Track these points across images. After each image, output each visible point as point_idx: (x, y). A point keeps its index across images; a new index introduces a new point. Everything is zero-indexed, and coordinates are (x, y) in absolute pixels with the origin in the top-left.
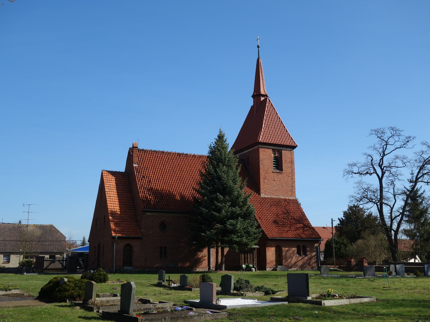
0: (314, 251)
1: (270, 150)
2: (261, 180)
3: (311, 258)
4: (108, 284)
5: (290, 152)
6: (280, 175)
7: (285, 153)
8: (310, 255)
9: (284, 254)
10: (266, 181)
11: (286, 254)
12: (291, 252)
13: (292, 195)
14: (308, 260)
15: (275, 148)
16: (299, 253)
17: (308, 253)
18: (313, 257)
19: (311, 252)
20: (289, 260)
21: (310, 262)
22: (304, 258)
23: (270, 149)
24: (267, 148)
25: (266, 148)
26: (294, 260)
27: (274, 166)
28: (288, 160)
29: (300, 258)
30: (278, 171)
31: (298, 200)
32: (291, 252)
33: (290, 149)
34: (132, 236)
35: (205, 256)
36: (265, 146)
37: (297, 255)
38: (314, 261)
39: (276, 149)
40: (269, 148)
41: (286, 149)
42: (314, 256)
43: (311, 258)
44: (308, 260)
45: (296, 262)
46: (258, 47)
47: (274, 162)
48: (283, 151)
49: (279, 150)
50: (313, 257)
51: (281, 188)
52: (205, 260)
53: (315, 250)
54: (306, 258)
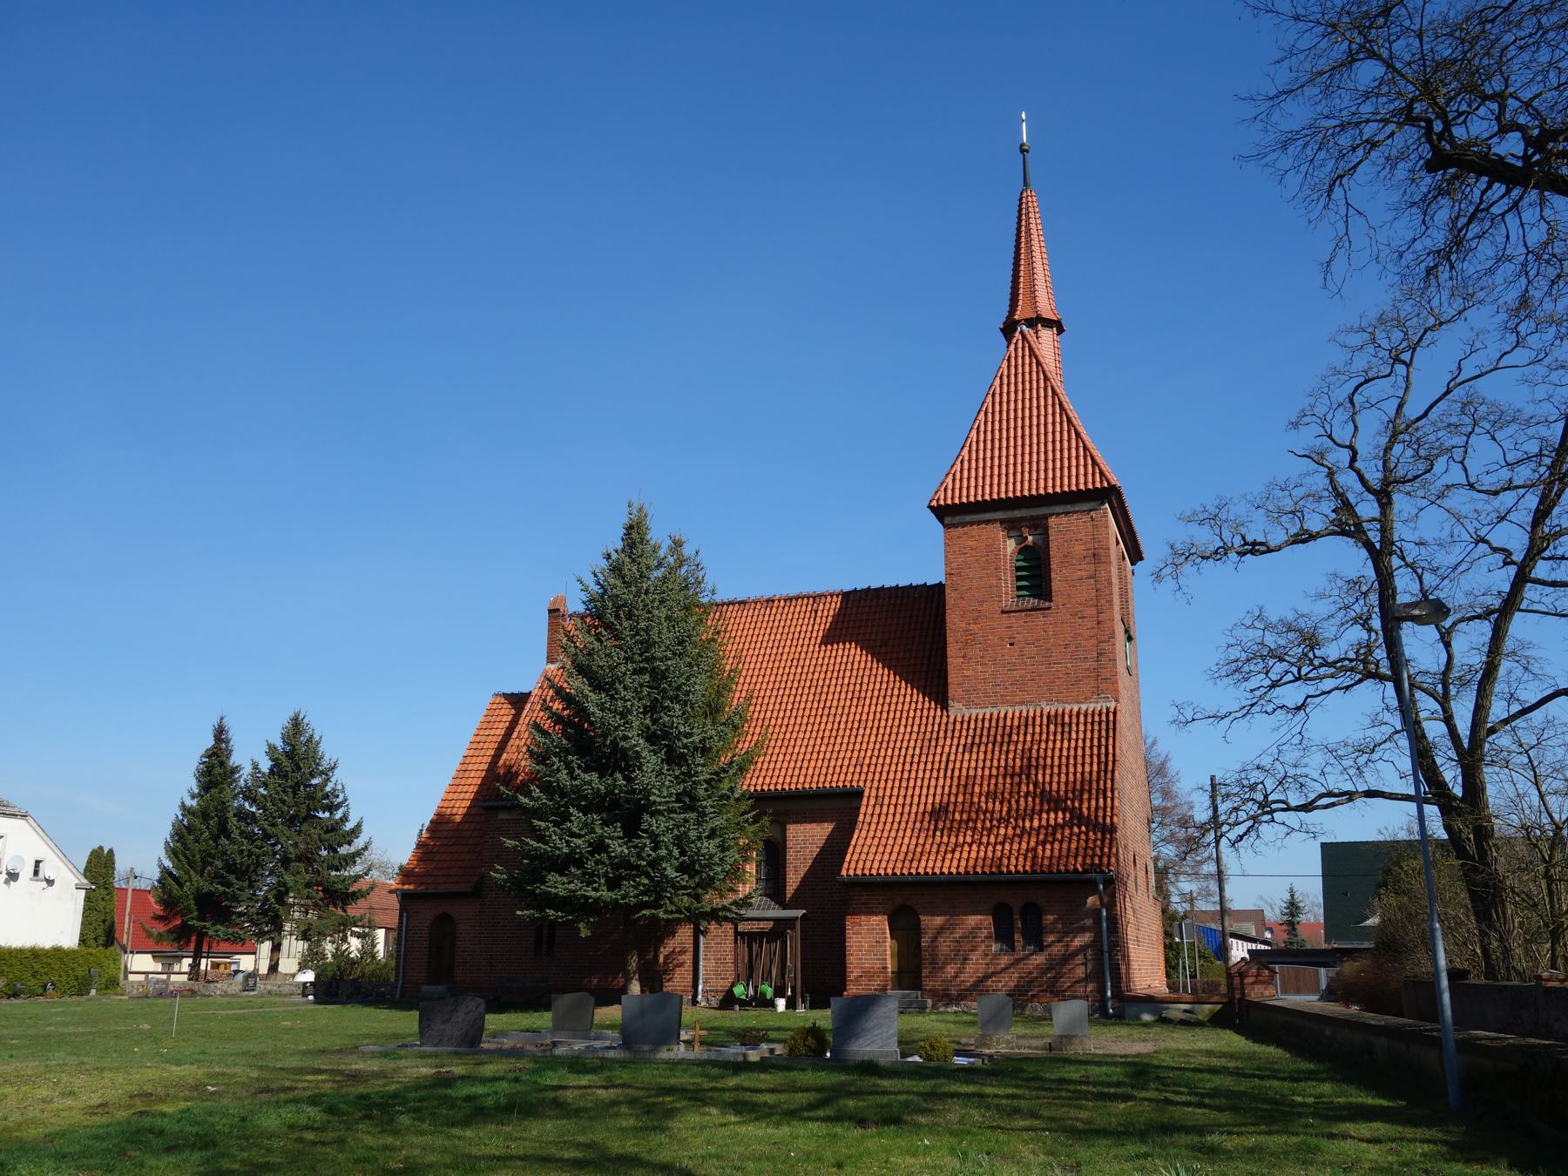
0: (1083, 930)
1: (991, 526)
2: (952, 649)
3: (1067, 958)
4: (1469, 986)
5: (1086, 518)
6: (1039, 618)
7: (1065, 530)
8: (1057, 949)
9: (925, 941)
10: (975, 651)
11: (935, 939)
12: (958, 933)
13: (1097, 693)
14: (1049, 969)
15: (1018, 514)
16: (1003, 934)
17: (1051, 938)
18: (1074, 954)
19: (1066, 934)
20: (950, 970)
21: (1059, 975)
22: (1027, 957)
23: (995, 521)
24: (979, 523)
25: (972, 523)
26: (975, 966)
27: (1019, 588)
28: (1079, 549)
29: (1005, 960)
30: (1034, 602)
31: (322, 748)
32: (958, 933)
33: (1086, 506)
34: (442, 889)
35: (682, 952)
36: (968, 518)
37: (995, 947)
38: (1080, 972)
39: (1022, 519)
40: (988, 522)
41: (1069, 508)
42: (1082, 949)
43: (1067, 958)
44: (1049, 969)
45: (986, 977)
46: (1023, 150)
47: (1018, 569)
48: (1052, 521)
49: (1032, 518)
50: (1074, 954)
51: (1043, 668)
52: (681, 965)
53: (1089, 922)
54: (1039, 959)
